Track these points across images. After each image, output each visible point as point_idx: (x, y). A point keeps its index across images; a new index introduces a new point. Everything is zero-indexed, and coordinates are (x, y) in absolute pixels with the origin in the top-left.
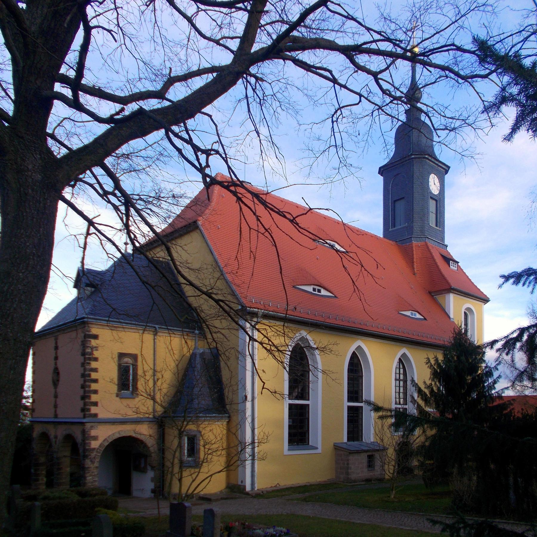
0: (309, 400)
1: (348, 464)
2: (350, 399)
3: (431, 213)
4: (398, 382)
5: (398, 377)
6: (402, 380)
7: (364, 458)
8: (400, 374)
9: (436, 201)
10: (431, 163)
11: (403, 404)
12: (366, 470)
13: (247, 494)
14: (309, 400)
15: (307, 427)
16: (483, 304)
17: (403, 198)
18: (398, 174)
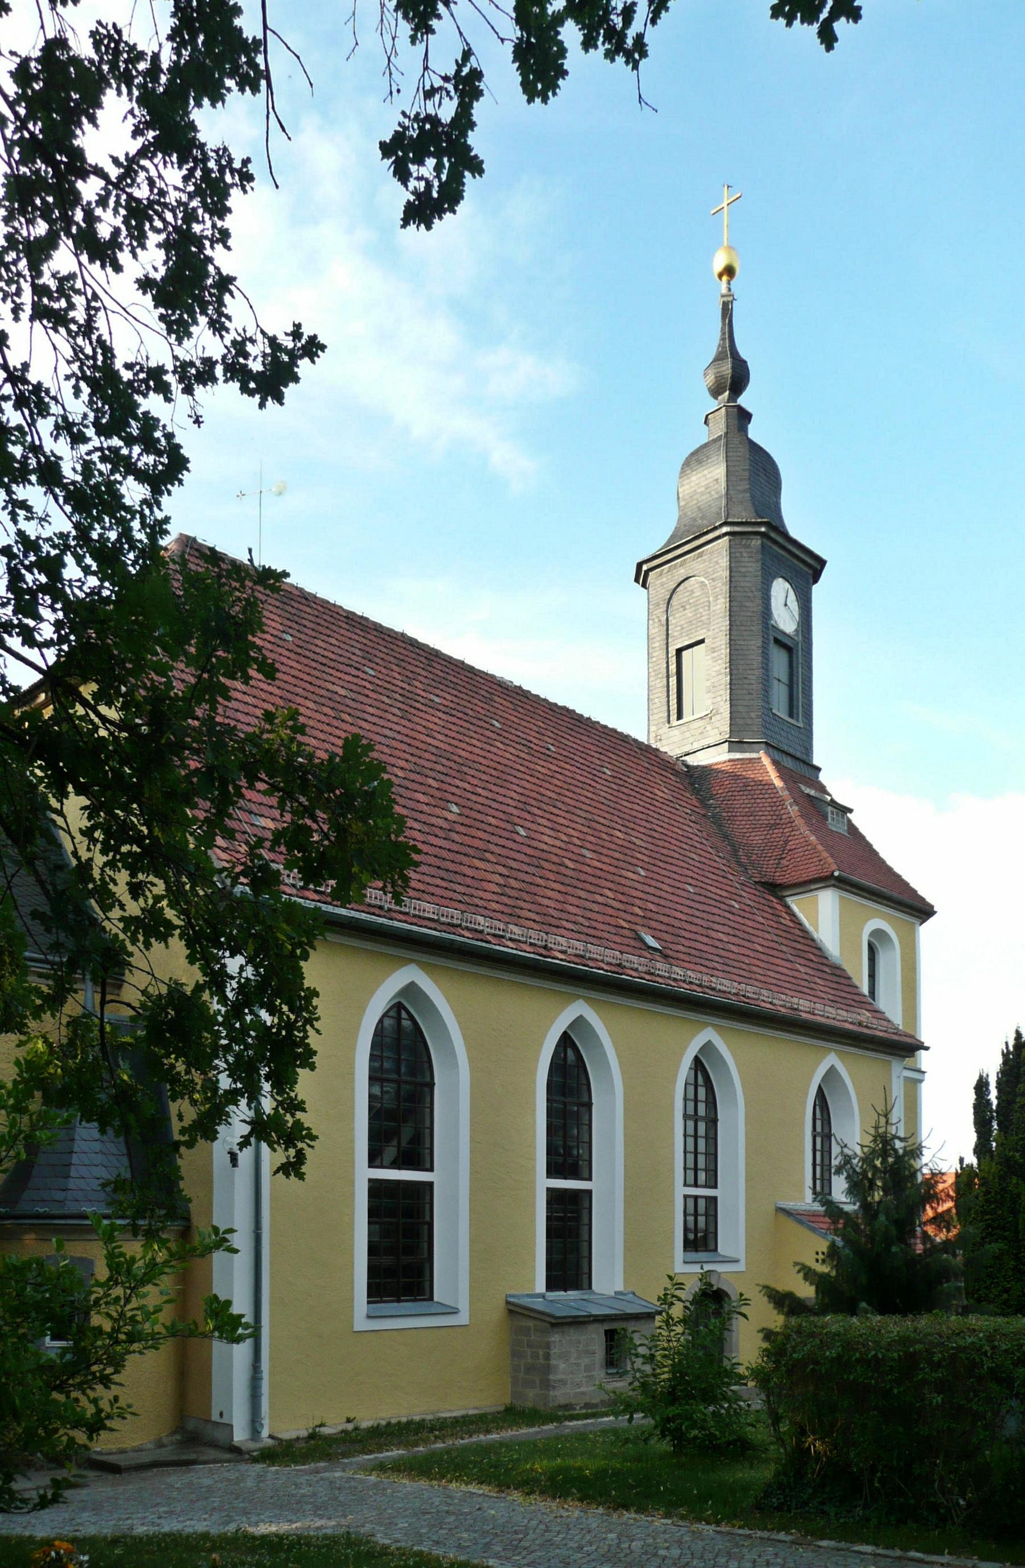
0: (431, 1169)
1: (547, 1357)
2: (553, 1171)
3: (776, 682)
4: (691, 1124)
5: (691, 1111)
6: (702, 1118)
7: (595, 1339)
8: (696, 1101)
9: (789, 650)
10: (775, 548)
11: (706, 1186)
12: (600, 1373)
13: (236, 1450)
14: (431, 1169)
15: (426, 1245)
16: (916, 921)
17: (702, 641)
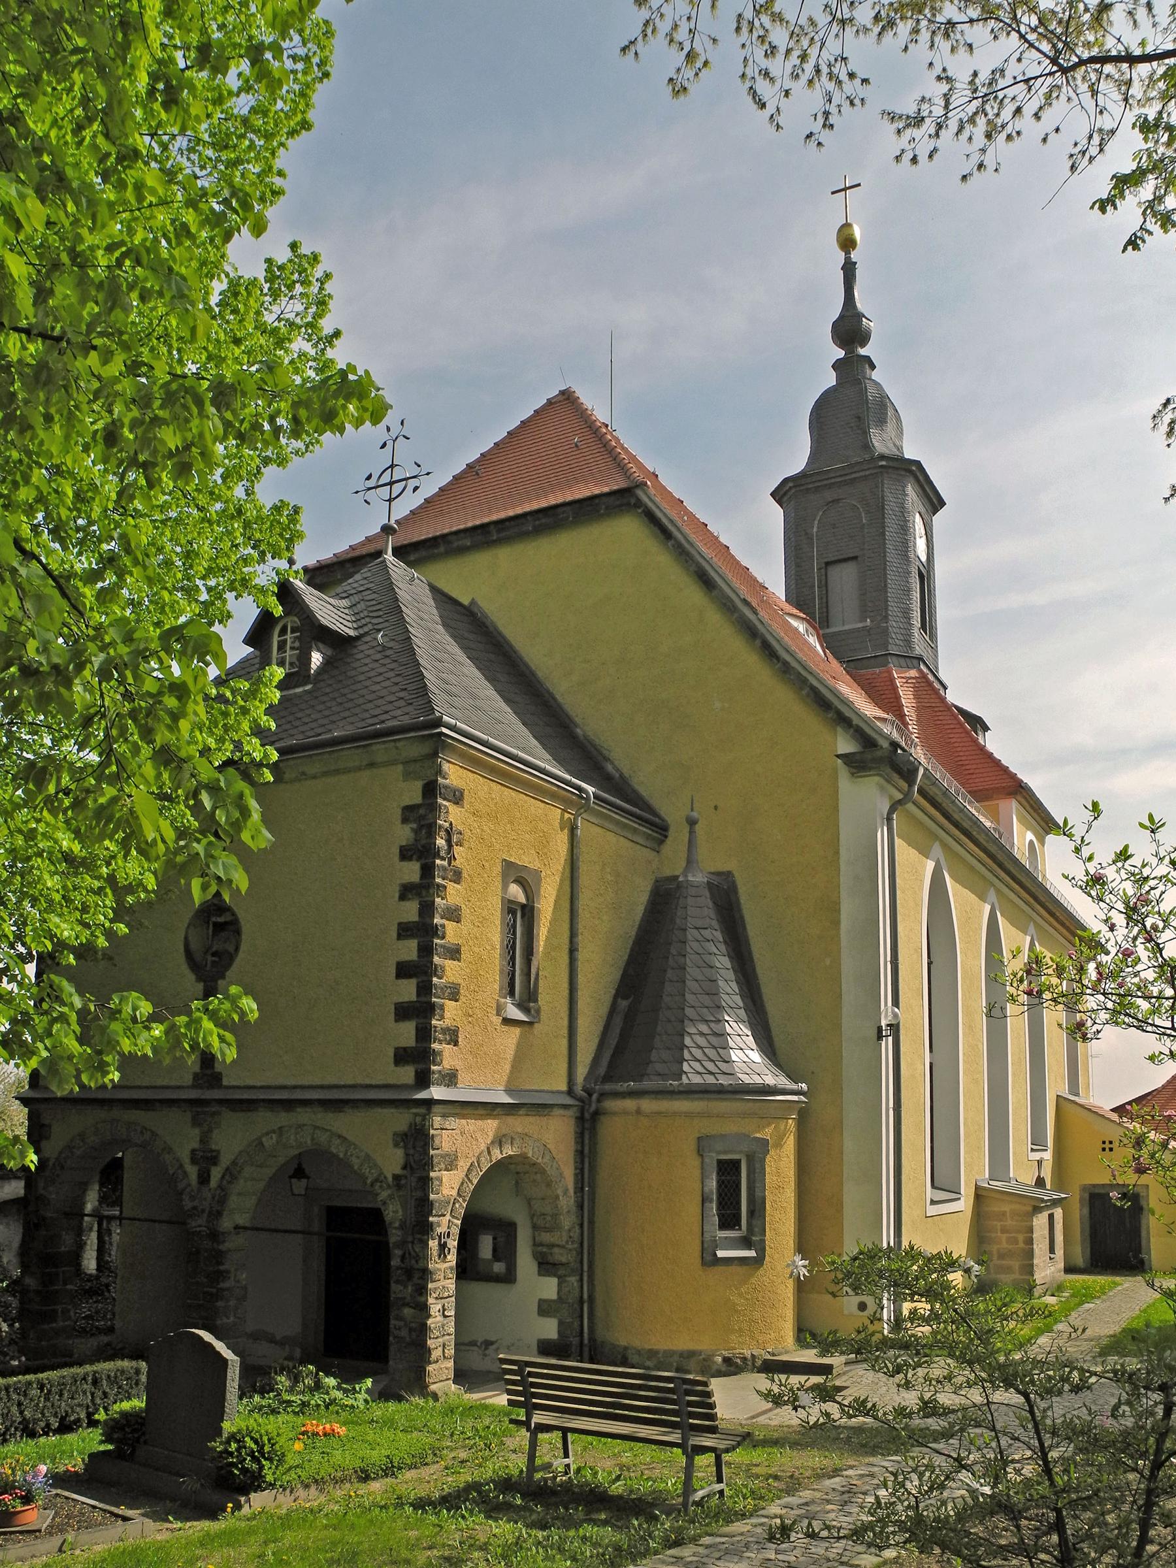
18: (837, 501)
